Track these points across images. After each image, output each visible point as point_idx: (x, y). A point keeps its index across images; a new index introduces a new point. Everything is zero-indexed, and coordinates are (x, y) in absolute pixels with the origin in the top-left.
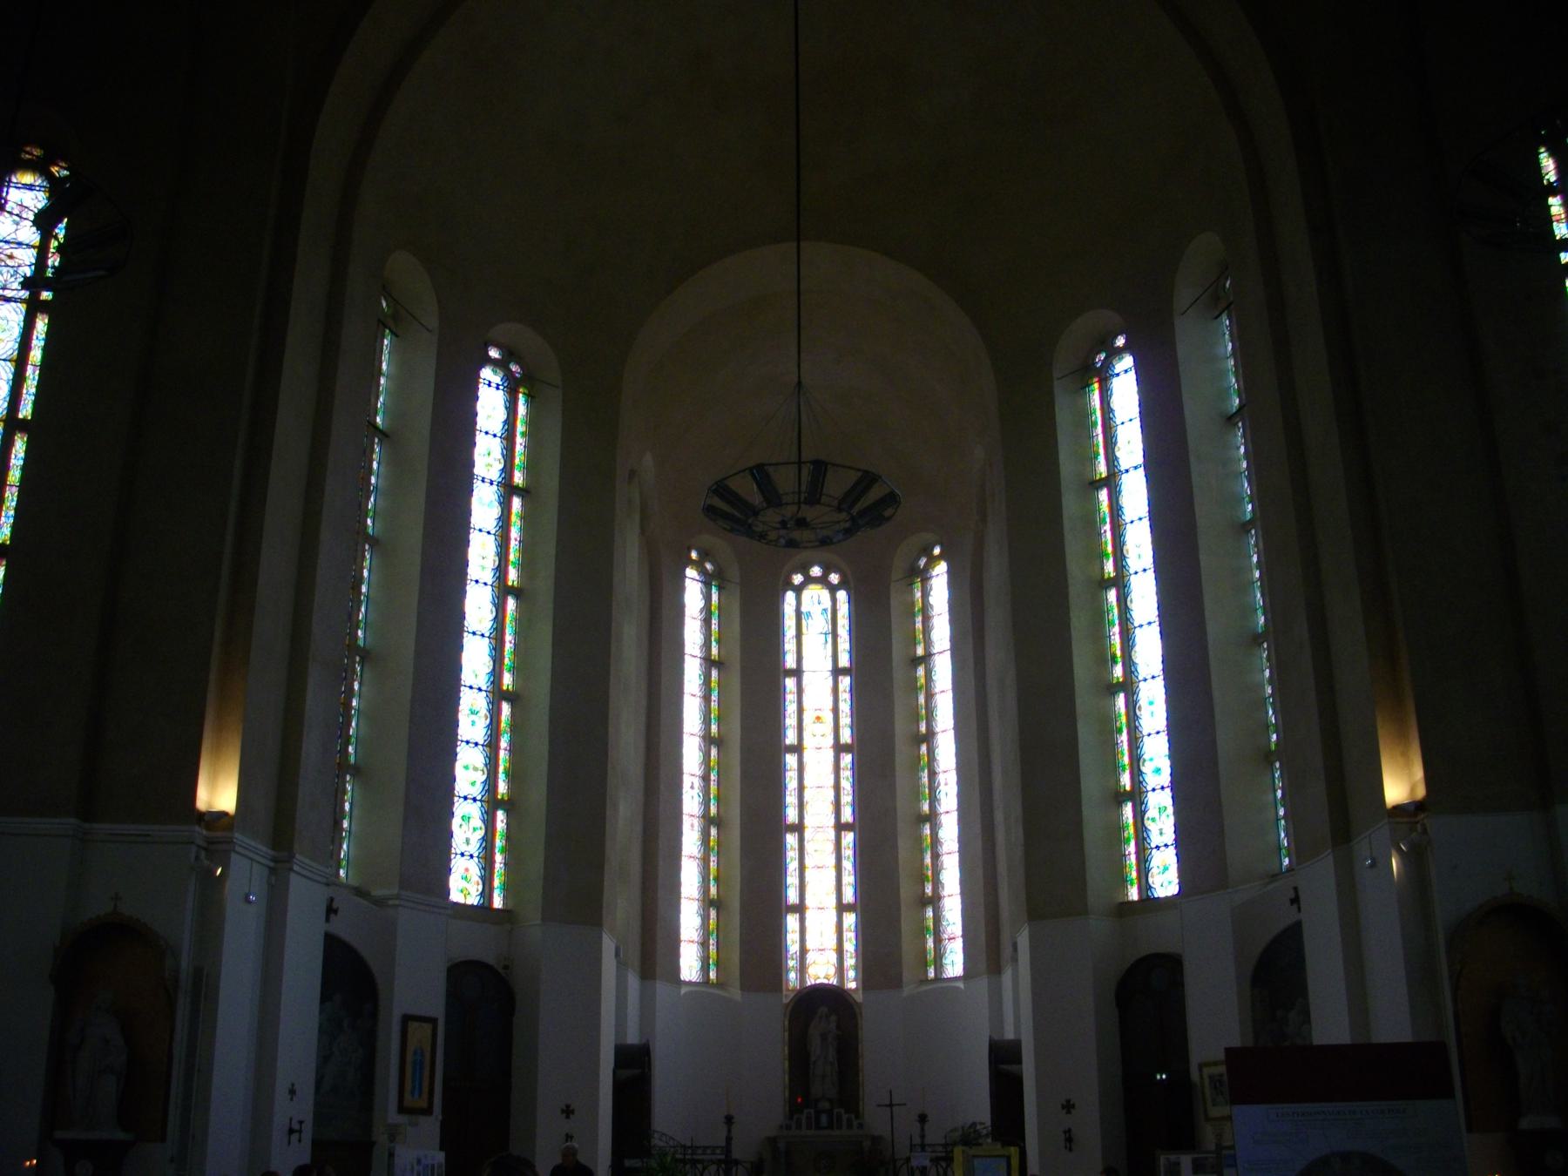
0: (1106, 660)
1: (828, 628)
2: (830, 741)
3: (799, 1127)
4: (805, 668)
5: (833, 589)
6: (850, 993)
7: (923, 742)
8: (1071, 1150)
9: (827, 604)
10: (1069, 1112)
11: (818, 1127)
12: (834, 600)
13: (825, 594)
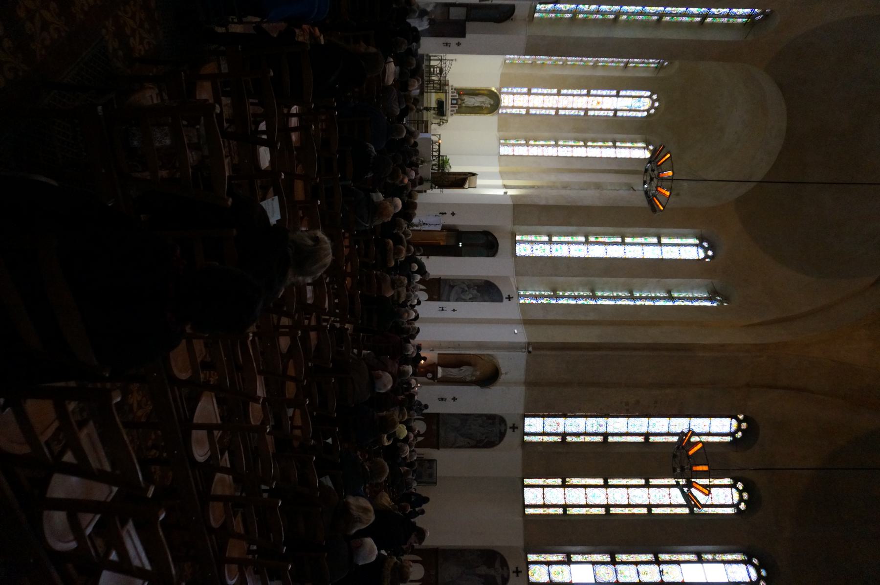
0: (596, 235)
1: (633, 108)
2: (589, 107)
3: (452, 93)
4: (619, 98)
5: (648, 111)
6: (497, 110)
7: (584, 143)
8: (446, 399)
9: (642, 108)
10: (453, 212)
11: (452, 100)
12: (644, 111)
13: (646, 107)
